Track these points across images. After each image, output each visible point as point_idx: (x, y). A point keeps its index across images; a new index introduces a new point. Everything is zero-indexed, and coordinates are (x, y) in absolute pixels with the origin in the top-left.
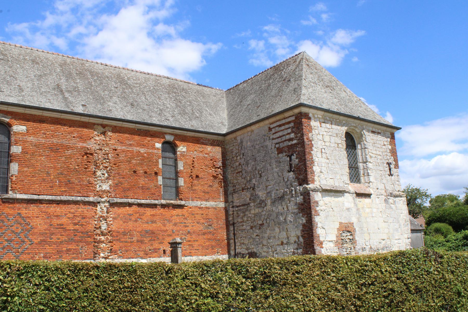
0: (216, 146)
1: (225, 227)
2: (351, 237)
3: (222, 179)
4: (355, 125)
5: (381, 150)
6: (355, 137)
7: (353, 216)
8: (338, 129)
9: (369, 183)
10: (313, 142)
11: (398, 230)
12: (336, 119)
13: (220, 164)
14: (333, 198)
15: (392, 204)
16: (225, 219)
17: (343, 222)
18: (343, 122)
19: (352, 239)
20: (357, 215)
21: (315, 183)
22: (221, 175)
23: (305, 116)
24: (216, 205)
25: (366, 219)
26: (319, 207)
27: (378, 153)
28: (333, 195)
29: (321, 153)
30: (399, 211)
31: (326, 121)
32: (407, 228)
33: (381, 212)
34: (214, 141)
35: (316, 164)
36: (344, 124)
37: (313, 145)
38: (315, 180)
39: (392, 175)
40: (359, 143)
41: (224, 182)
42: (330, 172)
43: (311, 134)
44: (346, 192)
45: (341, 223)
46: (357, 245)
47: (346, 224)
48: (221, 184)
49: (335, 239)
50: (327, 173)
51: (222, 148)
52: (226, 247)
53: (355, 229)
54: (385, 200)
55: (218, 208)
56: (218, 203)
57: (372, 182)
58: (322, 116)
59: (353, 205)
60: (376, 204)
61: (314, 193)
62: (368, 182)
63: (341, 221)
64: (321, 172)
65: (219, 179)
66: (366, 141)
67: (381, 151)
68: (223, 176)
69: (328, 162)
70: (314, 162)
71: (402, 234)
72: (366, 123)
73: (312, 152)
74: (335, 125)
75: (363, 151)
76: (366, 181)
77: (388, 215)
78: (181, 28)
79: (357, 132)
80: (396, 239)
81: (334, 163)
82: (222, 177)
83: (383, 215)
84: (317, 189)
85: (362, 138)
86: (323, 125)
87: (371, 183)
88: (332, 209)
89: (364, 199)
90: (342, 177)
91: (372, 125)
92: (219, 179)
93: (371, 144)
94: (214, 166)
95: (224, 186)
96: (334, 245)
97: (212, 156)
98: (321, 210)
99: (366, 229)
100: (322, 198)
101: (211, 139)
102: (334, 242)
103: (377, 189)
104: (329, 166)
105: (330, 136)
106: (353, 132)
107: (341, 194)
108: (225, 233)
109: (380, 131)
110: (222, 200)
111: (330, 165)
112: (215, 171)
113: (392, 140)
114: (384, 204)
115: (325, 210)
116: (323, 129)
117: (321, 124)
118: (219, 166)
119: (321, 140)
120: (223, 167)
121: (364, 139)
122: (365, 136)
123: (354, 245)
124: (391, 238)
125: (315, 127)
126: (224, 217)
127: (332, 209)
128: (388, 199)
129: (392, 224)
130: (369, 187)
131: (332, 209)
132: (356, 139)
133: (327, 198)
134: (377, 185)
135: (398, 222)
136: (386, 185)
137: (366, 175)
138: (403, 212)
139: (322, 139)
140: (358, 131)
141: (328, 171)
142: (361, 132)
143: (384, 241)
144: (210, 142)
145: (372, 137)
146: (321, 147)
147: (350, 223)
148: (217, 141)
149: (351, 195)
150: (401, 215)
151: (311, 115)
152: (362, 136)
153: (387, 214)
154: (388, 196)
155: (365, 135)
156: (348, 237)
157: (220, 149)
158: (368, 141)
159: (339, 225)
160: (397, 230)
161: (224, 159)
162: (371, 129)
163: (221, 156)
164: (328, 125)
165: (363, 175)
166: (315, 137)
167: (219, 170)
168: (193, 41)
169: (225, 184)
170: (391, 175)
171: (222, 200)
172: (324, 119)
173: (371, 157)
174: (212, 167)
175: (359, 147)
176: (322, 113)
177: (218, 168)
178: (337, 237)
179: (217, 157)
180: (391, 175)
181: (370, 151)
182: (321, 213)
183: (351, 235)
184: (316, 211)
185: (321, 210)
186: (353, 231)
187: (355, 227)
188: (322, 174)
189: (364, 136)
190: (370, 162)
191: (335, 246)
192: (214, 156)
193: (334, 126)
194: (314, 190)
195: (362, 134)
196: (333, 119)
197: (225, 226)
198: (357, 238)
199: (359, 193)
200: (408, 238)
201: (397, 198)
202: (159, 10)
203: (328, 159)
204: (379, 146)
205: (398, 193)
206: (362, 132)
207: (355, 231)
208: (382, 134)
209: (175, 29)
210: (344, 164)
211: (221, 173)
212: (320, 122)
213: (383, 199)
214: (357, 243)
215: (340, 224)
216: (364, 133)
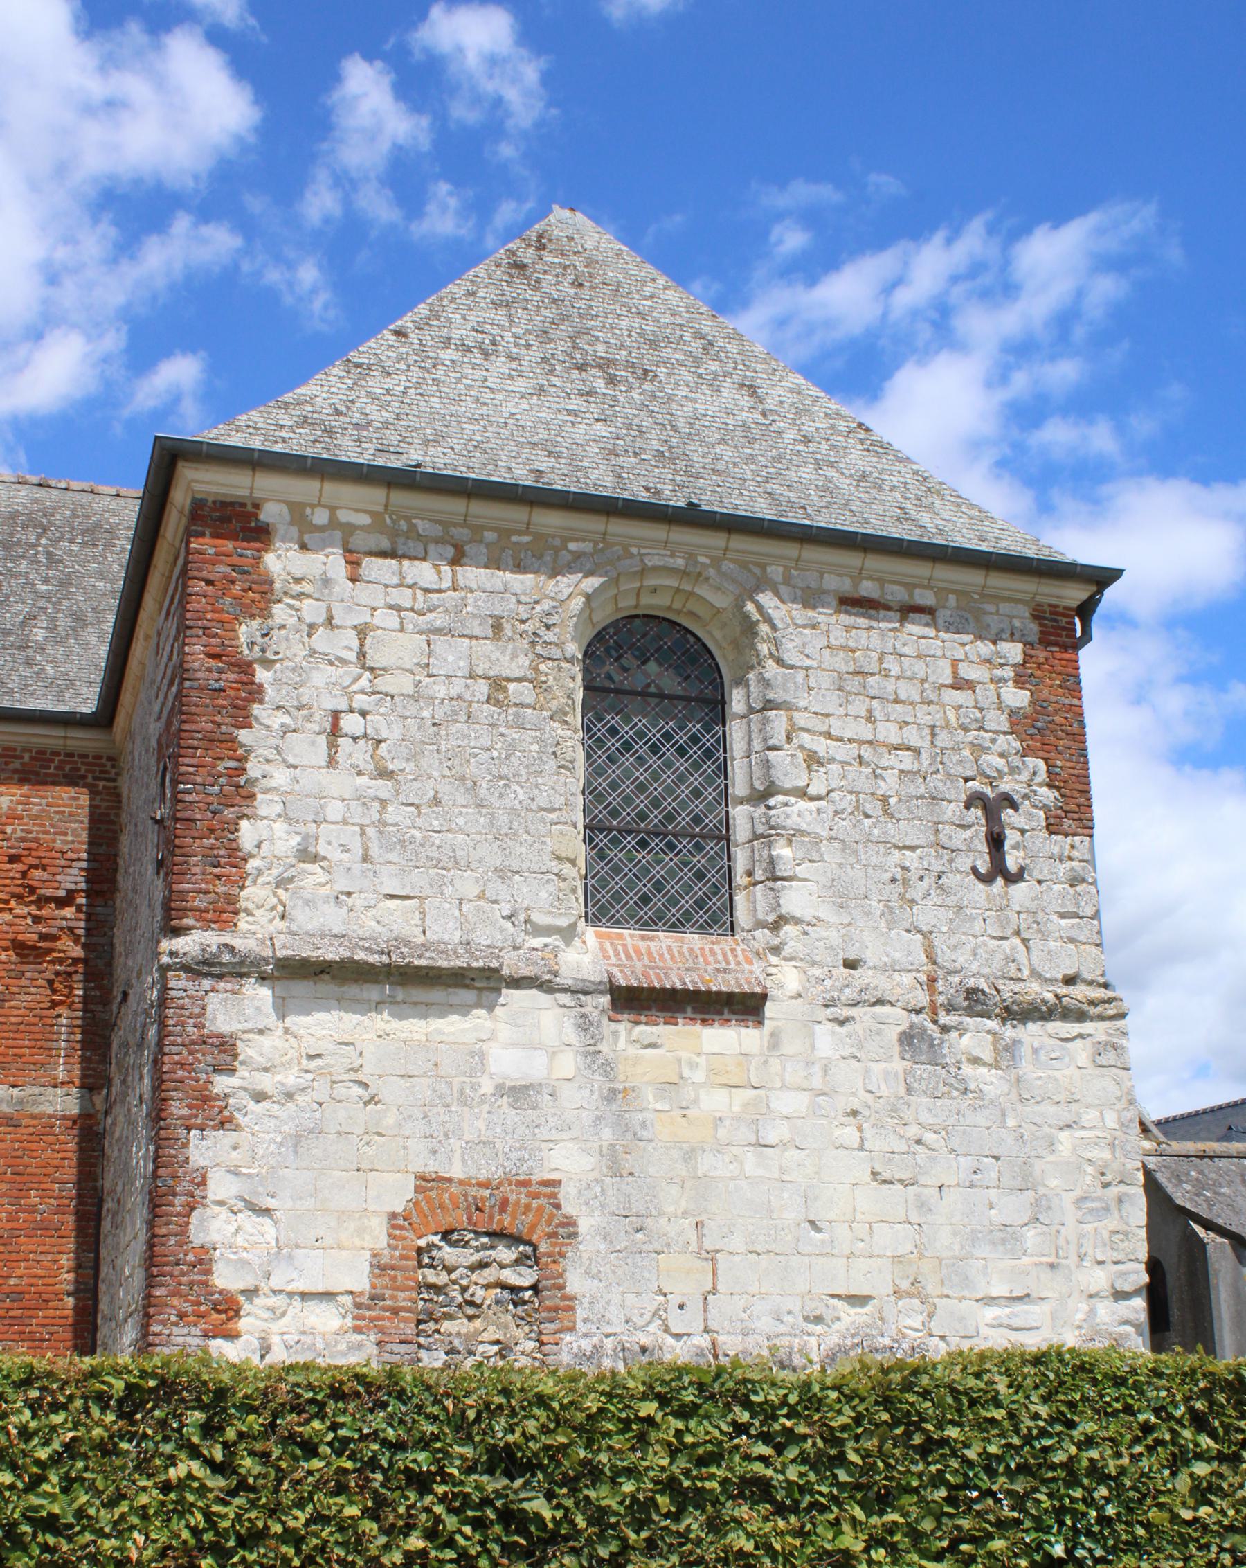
0: (54, 783)
1: (71, 1226)
2: (524, 1277)
3: (76, 961)
4: (680, 562)
5: (923, 715)
6: (715, 640)
7: (555, 1136)
8: (517, 587)
9: (775, 927)
10: (262, 675)
11: (1016, 1238)
12: (505, 533)
13: (74, 878)
14: (382, 1021)
15: (976, 1061)
16: (74, 1178)
17: (457, 1172)
18: (572, 546)
19: (534, 1288)
20: (607, 1134)
21: (243, 923)
22: (76, 940)
23: (225, 520)
24: (21, 1101)
25: (690, 1155)
26: (243, 1072)
27: (889, 733)
28: (393, 1002)
29: (323, 739)
30: (1048, 1109)
31: (414, 547)
32: (1113, 1223)
33: (854, 1113)
34: (42, 756)
35: (266, 805)
36: (578, 556)
37: (256, 693)
38: (243, 904)
39: (1013, 878)
40: (741, 681)
41: (89, 977)
42: (393, 857)
43: (255, 623)
44: (517, 983)
45: (426, 1183)
46: (572, 1329)
47: (485, 1185)
48: (71, 988)
49: (360, 1280)
50: (366, 859)
51: (94, 792)
52: (69, 1336)
53: (570, 1222)
54: (908, 1039)
55: (33, 1117)
56: (36, 1090)
57: (797, 921)
58: (373, 514)
59: (568, 1064)
60: (809, 1063)
61: (206, 983)
62: (771, 918)
63: (432, 1167)
64: (307, 855)
65: (61, 961)
66: (780, 662)
67: (928, 720)
68: (84, 946)
69: (384, 795)
70: (252, 796)
71: (1052, 1266)
72: (790, 550)
73: (243, 735)
74: (494, 563)
75: (754, 728)
76: (761, 916)
77: (929, 1137)
78: (1144, 425)
79: (718, 611)
80: (990, 1300)
81: (436, 801)
82: (78, 952)
83: (869, 1132)
84: (226, 958)
85: (753, 646)
86: (376, 568)
87: (788, 930)
88: (365, 1085)
89: (698, 1027)
90: (496, 888)
91: (852, 559)
92: (61, 961)
93: (823, 680)
94: (32, 890)
95: (86, 999)
96: (349, 1322)
97: (23, 840)
98: (259, 1097)
99: (688, 1223)
100: (282, 1017)
101: (24, 750)
102: (347, 1300)
103: (851, 964)
104: (389, 818)
105: (438, 631)
106: (692, 614)
107: (468, 996)
108: (66, 1261)
109: (925, 598)
110: (61, 1075)
111: (394, 813)
112: (37, 919)
113: (1041, 654)
114: (899, 1066)
115: (289, 1096)
116: (364, 593)
117: (354, 564)
118: (62, 893)
119: (343, 661)
120: (89, 893)
121: (764, 648)
122: (774, 628)
123: (548, 1327)
124: (931, 1287)
125: (298, 581)
126: (69, 1170)
127: (357, 1090)
128: (945, 1029)
129: (953, 1197)
130: (776, 950)
131: (365, 1085)
132: (724, 657)
133: (321, 1016)
134: (848, 939)
135: (1027, 1182)
136: (938, 941)
137: (759, 874)
138: (1090, 1116)
139: (352, 656)
140: (721, 601)
141: (375, 851)
142: (740, 607)
143: (868, 1309)
144: (17, 764)
145: (838, 637)
146: (330, 704)
147: (525, 1184)
148: (71, 755)
149: (564, 998)
150: (1064, 1136)
151: (271, 513)
152: (750, 629)
153: (913, 1131)
154: (950, 1008)
155: (769, 620)
156: (489, 1275)
157: (85, 799)
158: (791, 657)
159: (410, 1194)
160: (1006, 1237)
161: (102, 850)
162: (832, 582)
163: (84, 836)
164: (426, 566)
165: (746, 880)
166: (290, 647)
167: (69, 912)
168: (1204, 477)
169: (97, 988)
170: (998, 871)
171: (61, 1075)
172: (394, 534)
173: (813, 760)
174: (19, 897)
175: (737, 702)
176: (374, 496)
177: (62, 903)
178: (380, 1268)
179: (58, 845)
180: (998, 871)
181: (801, 719)
182: (250, 1114)
183: (531, 1258)
184: (205, 1099)
185: (259, 1097)
186: (554, 1235)
187: (568, 1208)
188: (315, 868)
189: (764, 629)
190: (802, 793)
191: (358, 1330)
192: (36, 840)
193: (471, 575)
194: (206, 963)
195: (746, 617)
196: (478, 530)
197: (72, 1219)
198: (575, 1283)
199: (630, 989)
200: (1120, 1296)
201: (1032, 1027)
202: (1053, 358)
203: (384, 774)
204: (907, 691)
205: (1036, 991)
206: (750, 607)
207: (574, 1235)
208: (943, 615)
209: (1120, 430)
210: (542, 801)
211: (71, 929)
212: (348, 550)
213: (892, 1033)
214: (580, 1313)
215: (417, 1190)
216: (760, 608)
